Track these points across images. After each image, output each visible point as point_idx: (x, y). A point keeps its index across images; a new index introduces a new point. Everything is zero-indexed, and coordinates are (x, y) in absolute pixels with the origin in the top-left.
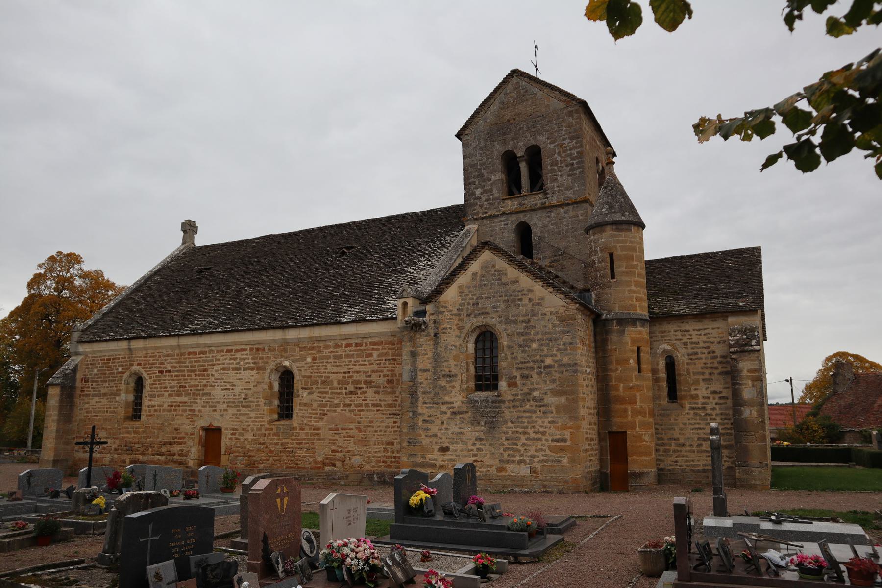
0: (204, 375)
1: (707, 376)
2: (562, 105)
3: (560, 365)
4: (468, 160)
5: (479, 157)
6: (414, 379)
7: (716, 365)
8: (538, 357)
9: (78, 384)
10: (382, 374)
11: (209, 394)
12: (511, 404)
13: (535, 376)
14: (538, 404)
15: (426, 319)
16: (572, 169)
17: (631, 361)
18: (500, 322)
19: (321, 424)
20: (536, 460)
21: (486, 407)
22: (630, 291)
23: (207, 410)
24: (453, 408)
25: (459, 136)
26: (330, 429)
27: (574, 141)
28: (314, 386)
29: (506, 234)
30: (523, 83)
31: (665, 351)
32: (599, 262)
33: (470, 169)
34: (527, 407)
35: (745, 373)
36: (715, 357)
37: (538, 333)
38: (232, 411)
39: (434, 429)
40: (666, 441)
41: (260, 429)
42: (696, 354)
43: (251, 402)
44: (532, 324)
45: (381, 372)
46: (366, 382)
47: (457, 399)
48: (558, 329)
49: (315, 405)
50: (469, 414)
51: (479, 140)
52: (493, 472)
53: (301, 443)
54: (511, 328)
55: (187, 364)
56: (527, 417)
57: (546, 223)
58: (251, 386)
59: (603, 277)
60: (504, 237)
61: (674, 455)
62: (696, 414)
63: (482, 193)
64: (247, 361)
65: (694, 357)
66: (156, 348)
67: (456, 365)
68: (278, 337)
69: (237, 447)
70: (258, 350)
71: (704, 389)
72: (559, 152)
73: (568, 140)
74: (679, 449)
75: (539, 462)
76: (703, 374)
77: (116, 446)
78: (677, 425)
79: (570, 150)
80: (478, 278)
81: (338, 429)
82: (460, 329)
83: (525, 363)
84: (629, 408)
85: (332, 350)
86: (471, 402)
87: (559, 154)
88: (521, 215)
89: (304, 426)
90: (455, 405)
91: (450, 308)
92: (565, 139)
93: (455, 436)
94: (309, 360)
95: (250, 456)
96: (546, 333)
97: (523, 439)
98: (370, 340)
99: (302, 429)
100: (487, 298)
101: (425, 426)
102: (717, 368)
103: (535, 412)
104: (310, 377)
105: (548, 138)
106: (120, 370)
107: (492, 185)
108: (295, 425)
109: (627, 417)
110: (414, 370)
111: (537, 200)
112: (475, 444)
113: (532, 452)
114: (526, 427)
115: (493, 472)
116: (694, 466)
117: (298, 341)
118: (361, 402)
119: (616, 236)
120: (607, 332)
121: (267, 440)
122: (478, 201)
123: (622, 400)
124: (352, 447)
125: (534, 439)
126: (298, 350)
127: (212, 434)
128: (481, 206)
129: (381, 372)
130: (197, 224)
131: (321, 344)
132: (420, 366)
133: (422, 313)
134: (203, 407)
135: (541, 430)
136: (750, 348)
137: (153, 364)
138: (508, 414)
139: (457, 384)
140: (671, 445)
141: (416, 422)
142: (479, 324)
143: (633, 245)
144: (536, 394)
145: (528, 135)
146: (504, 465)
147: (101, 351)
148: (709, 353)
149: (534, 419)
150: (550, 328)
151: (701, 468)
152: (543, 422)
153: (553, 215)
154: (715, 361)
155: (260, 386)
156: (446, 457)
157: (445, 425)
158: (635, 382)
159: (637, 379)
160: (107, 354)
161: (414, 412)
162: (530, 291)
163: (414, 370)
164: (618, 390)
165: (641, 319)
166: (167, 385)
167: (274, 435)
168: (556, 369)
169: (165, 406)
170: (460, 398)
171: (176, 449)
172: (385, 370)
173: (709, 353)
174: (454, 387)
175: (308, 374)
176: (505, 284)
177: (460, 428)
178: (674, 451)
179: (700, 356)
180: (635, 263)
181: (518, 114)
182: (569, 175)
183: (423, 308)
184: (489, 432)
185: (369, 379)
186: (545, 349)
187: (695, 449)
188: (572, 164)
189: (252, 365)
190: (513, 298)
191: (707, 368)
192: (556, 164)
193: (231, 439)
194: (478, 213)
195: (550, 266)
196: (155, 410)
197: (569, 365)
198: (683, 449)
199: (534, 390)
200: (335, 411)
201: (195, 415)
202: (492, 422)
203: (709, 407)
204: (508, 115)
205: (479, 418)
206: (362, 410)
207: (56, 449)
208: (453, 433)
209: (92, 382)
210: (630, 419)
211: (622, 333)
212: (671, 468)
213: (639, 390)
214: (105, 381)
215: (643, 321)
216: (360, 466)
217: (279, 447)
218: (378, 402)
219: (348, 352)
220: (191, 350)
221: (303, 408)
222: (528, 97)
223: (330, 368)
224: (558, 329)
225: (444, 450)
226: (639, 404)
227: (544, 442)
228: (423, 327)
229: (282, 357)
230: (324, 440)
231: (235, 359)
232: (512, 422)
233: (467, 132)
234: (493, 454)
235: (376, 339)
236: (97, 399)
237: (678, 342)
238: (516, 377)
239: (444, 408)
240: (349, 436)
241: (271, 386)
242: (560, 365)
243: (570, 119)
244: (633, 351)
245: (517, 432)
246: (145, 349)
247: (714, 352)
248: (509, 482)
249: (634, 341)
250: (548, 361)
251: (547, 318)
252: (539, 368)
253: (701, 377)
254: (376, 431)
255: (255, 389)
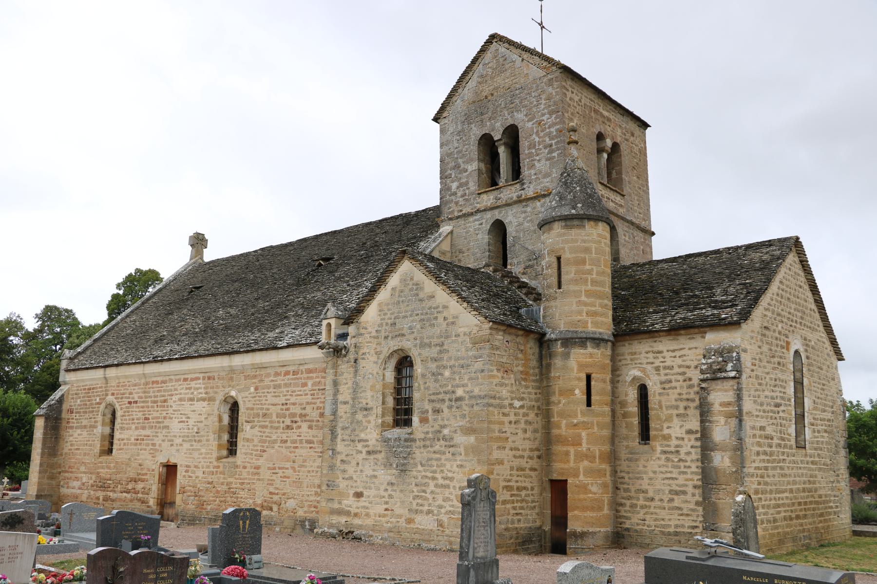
0: (164, 406)
1: (682, 411)
2: (542, 73)
3: (471, 397)
4: (446, 148)
5: (456, 145)
6: (334, 413)
7: (692, 396)
8: (449, 387)
9: (64, 415)
10: (315, 406)
11: (167, 427)
12: (422, 443)
13: (446, 410)
14: (448, 443)
15: (349, 342)
16: (550, 152)
17: (577, 392)
18: (415, 346)
19: (261, 462)
20: (443, 511)
21: (398, 446)
22: (580, 303)
23: (166, 444)
24: (367, 446)
25: (436, 119)
26: (269, 468)
27: (554, 116)
28: (256, 419)
29: (480, 236)
30: (502, 49)
31: (635, 379)
32: (547, 268)
33: (447, 160)
34: (437, 448)
35: (716, 407)
36: (691, 387)
37: (450, 358)
38: (186, 446)
39: (351, 470)
40: (633, 494)
41: (208, 467)
42: (670, 381)
43: (203, 436)
44: (445, 347)
45: (315, 403)
46: (301, 415)
47: (372, 435)
48: (470, 353)
49: (256, 442)
50: (383, 455)
51: (456, 123)
52: (402, 523)
53: (243, 483)
54: (427, 352)
55: (151, 394)
56: (437, 459)
57: (521, 220)
58: (202, 418)
59: (549, 287)
60: (477, 240)
61: (643, 511)
62: (668, 460)
63: (458, 188)
64: (200, 391)
65: (667, 386)
66: (126, 377)
67: (373, 396)
68: (225, 365)
69: (190, 486)
70: (209, 378)
71: (678, 428)
72: (537, 131)
73: (547, 116)
74: (647, 503)
75: (446, 513)
76: (677, 407)
77: (91, 482)
78: (646, 473)
79: (549, 128)
80: (397, 295)
81: (274, 469)
82: (378, 353)
83: (437, 394)
84: (572, 450)
85: (272, 378)
86: (386, 441)
87: (537, 133)
88: (496, 212)
89: (246, 464)
90: (369, 443)
91: (370, 330)
92: (543, 115)
93: (368, 480)
94: (252, 390)
95: (200, 496)
96: (457, 359)
97: (432, 487)
98: (306, 367)
99: (245, 467)
100: (405, 317)
101: (343, 467)
102: (693, 400)
103: (444, 453)
104: (252, 409)
105: (526, 115)
106: (98, 400)
107: (467, 177)
108: (239, 463)
109: (568, 461)
110: (335, 402)
111: (510, 193)
112: (386, 490)
113: (440, 502)
114: (435, 472)
115: (402, 523)
116: (664, 526)
117: (243, 369)
118: (296, 438)
119: (564, 234)
120: (551, 356)
121: (214, 478)
122: (453, 197)
123: (563, 441)
124: (288, 490)
125: (442, 486)
126: (243, 378)
127: (171, 470)
128: (457, 203)
129: (315, 403)
130: (206, 237)
131: (263, 372)
132: (341, 398)
133: (343, 336)
134: (163, 441)
135: (450, 475)
136: (723, 375)
137: (124, 394)
138: (420, 455)
139: (372, 418)
140: (638, 499)
141: (334, 461)
142: (396, 348)
143: (586, 245)
144: (446, 431)
145: (506, 113)
146: (413, 516)
147: (83, 381)
148: (685, 381)
149: (443, 461)
150: (462, 353)
151: (672, 530)
152: (451, 467)
153: (529, 209)
154: (692, 391)
155: (210, 418)
156: (361, 504)
157: (360, 467)
158: (581, 418)
159: (583, 414)
160: (88, 383)
161: (333, 450)
162: (445, 307)
163: (335, 402)
164: (559, 427)
165: (593, 339)
166: (135, 417)
167: (221, 473)
168: (467, 402)
169: (132, 440)
170: (375, 436)
171: (140, 486)
172: (318, 401)
173: (685, 381)
174: (369, 422)
175: (250, 406)
176: (421, 300)
177: (374, 470)
178: (642, 507)
179: (674, 384)
180: (588, 267)
181: (496, 89)
182: (547, 160)
183: (345, 331)
184: (400, 476)
185: (303, 412)
186: (457, 378)
187: (665, 504)
188: (551, 146)
189: (204, 395)
190: (428, 319)
191: (681, 400)
192: (534, 146)
193: (184, 476)
194: (453, 212)
195: (524, 273)
196: (124, 444)
197: (480, 397)
198: (653, 504)
199: (444, 427)
200: (273, 447)
201: (156, 450)
202: (403, 465)
203: (683, 451)
204: (486, 90)
205: (392, 459)
206: (297, 447)
207: (39, 484)
208: (367, 476)
209: (77, 413)
210: (572, 464)
211: (567, 356)
212: (638, 528)
213: (583, 430)
214: (86, 412)
215: (597, 341)
216: (294, 511)
217: (225, 487)
218: (311, 438)
219: (286, 381)
220: (155, 379)
221: (246, 444)
222: (507, 66)
223: (271, 399)
224: (470, 353)
225: (359, 495)
226: (585, 446)
227: (452, 490)
228: (343, 352)
229: (230, 386)
230: (263, 480)
231: (190, 388)
232: (422, 465)
233: (445, 115)
234: (403, 502)
235: (311, 366)
236: (79, 431)
237: (649, 367)
238: (427, 411)
239: (359, 446)
240: (285, 477)
241: (220, 420)
242: (471, 397)
243: (550, 89)
244: (579, 379)
245: (426, 477)
246: (118, 378)
247: (690, 379)
248: (417, 536)
249: (581, 366)
250: (460, 392)
251: (460, 340)
252: (450, 400)
253: (675, 412)
254: (309, 471)
255: (205, 422)
